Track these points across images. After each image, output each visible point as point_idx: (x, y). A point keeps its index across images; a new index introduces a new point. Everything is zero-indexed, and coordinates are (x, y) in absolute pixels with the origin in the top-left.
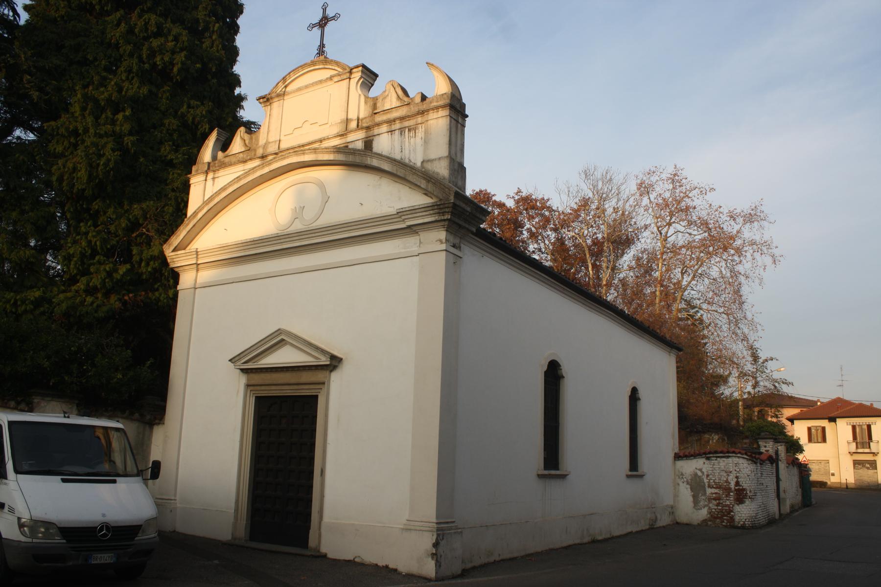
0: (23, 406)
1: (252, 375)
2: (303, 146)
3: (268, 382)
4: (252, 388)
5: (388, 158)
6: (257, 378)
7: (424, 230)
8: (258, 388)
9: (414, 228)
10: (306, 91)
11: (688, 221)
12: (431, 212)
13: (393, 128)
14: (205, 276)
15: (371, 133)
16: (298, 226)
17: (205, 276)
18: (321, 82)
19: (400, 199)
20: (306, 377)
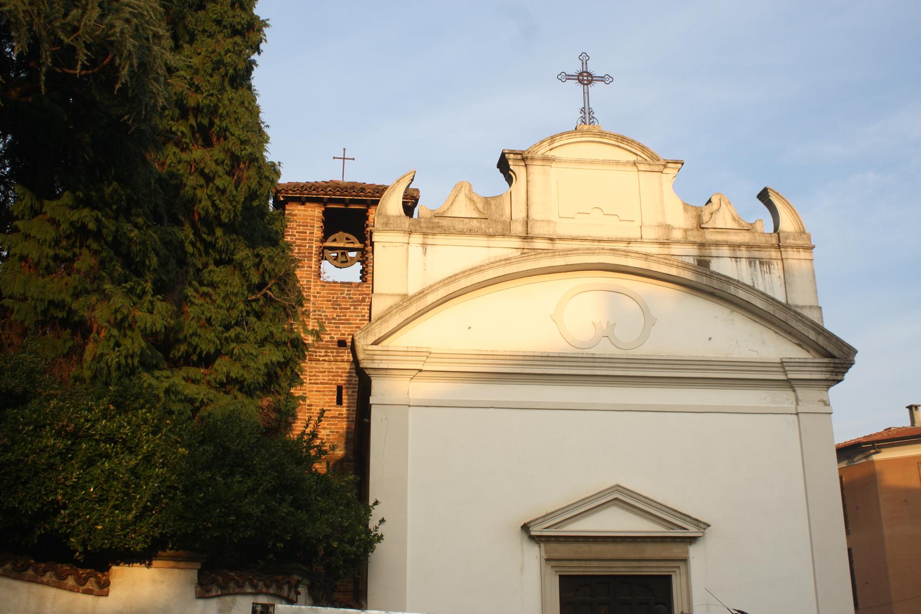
0: (48, 576)
1: (553, 546)
2: (599, 241)
3: (587, 556)
4: (554, 563)
5: (763, 294)
6: (564, 550)
7: (804, 386)
8: (567, 564)
9: (793, 383)
10: (588, 166)
11: (325, 452)
12: (824, 369)
13: (738, 254)
14: (421, 390)
15: (707, 252)
16: (605, 349)
17: (421, 390)
18: (617, 163)
19: (764, 343)
20: (651, 551)
